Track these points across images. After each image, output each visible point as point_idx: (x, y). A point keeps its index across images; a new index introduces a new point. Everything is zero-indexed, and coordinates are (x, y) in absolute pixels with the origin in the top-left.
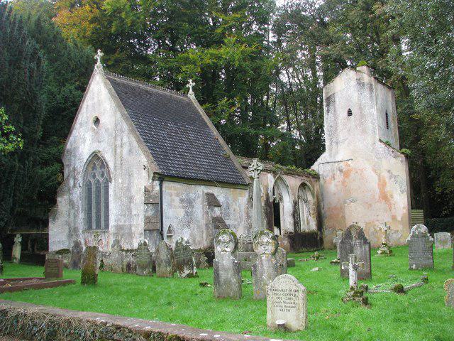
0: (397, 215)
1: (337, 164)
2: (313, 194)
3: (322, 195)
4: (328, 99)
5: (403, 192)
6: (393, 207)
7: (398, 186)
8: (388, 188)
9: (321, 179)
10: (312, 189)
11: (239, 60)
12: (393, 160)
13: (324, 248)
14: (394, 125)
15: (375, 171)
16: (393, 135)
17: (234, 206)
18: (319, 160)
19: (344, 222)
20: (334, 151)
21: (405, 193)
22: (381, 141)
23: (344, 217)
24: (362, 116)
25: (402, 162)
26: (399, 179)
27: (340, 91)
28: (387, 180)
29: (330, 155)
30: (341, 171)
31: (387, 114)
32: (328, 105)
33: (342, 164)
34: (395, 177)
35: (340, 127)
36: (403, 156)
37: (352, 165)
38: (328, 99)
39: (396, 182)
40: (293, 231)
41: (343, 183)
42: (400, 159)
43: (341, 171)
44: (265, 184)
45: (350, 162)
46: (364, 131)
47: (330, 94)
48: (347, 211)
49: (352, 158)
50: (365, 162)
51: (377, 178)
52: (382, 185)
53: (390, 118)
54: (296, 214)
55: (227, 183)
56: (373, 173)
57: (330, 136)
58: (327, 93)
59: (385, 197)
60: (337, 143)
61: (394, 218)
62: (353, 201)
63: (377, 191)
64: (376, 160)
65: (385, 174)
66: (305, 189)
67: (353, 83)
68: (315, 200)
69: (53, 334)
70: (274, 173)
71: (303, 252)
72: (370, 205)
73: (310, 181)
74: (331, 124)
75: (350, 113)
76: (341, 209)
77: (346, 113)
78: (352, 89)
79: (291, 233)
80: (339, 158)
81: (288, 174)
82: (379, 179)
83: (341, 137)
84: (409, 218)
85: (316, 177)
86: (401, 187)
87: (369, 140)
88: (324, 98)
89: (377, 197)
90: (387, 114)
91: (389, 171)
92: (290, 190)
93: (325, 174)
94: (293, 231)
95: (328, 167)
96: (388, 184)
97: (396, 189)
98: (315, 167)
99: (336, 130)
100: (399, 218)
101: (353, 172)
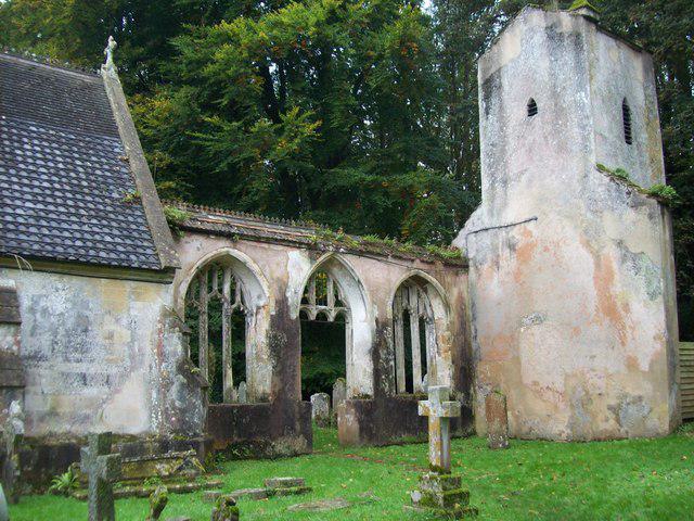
0: (640, 356)
1: (503, 233)
2: (447, 306)
3: (473, 305)
4: (488, 82)
5: (652, 296)
6: (629, 335)
7: (641, 281)
8: (617, 288)
9: (472, 269)
10: (442, 290)
11: (318, 24)
12: (630, 214)
13: (474, 433)
14: (649, 135)
15: (587, 244)
16: (646, 158)
17: (110, 326)
18: (469, 225)
19: (519, 371)
20: (498, 201)
21: (660, 299)
22: (600, 168)
23: (517, 361)
24: (559, 112)
25: (651, 217)
26: (645, 263)
27: (512, 60)
28: (615, 266)
29: (491, 213)
30: (512, 247)
31: (626, 110)
32: (487, 98)
33: (515, 233)
34: (636, 257)
35: (512, 143)
36: (653, 201)
37: (535, 232)
38: (488, 82)
39: (638, 270)
40: (370, 393)
41: (517, 275)
42: (645, 210)
43: (512, 247)
44: (278, 274)
45: (531, 226)
46: (562, 148)
47: (493, 70)
48: (524, 346)
49: (537, 215)
50: (565, 222)
51: (591, 260)
52: (604, 278)
53: (638, 120)
54: (383, 353)
55: (76, 262)
56: (584, 252)
57: (490, 166)
58: (484, 72)
59: (612, 311)
60: (505, 182)
61: (632, 364)
62: (539, 320)
63: (593, 292)
64: (589, 215)
65: (612, 252)
66: (426, 291)
67: (540, 37)
68: (453, 315)
69: (686, 366)
70: (312, 249)
71: (401, 444)
72: (577, 331)
73: (436, 275)
74: (494, 139)
75: (532, 109)
76: (512, 339)
77: (524, 110)
78: (537, 52)
79: (367, 396)
80: (510, 216)
81: (360, 254)
82: (598, 265)
83: (513, 169)
84: (672, 366)
85: (459, 265)
86: (649, 283)
87: (575, 166)
88: (480, 82)
89: (591, 308)
90: (626, 110)
91: (620, 244)
92: (366, 293)
93: (479, 257)
94: (370, 393)
95: (486, 239)
96: (617, 277)
97: (637, 290)
98: (458, 242)
99: (503, 151)
100: (644, 366)
101: (539, 249)
